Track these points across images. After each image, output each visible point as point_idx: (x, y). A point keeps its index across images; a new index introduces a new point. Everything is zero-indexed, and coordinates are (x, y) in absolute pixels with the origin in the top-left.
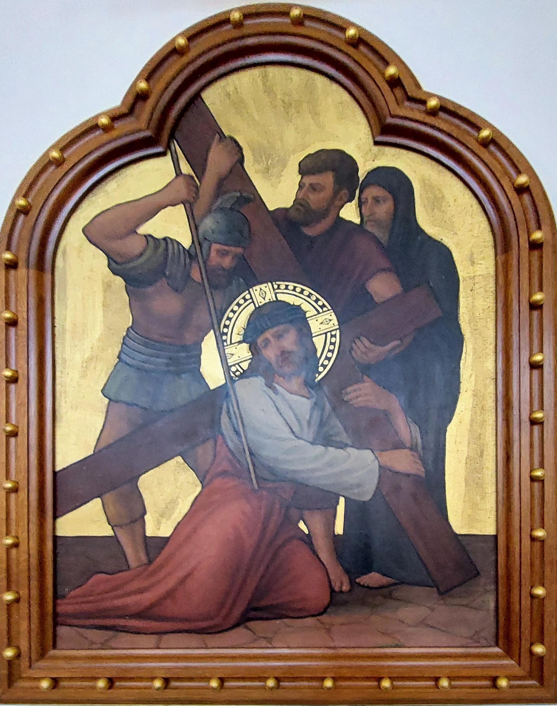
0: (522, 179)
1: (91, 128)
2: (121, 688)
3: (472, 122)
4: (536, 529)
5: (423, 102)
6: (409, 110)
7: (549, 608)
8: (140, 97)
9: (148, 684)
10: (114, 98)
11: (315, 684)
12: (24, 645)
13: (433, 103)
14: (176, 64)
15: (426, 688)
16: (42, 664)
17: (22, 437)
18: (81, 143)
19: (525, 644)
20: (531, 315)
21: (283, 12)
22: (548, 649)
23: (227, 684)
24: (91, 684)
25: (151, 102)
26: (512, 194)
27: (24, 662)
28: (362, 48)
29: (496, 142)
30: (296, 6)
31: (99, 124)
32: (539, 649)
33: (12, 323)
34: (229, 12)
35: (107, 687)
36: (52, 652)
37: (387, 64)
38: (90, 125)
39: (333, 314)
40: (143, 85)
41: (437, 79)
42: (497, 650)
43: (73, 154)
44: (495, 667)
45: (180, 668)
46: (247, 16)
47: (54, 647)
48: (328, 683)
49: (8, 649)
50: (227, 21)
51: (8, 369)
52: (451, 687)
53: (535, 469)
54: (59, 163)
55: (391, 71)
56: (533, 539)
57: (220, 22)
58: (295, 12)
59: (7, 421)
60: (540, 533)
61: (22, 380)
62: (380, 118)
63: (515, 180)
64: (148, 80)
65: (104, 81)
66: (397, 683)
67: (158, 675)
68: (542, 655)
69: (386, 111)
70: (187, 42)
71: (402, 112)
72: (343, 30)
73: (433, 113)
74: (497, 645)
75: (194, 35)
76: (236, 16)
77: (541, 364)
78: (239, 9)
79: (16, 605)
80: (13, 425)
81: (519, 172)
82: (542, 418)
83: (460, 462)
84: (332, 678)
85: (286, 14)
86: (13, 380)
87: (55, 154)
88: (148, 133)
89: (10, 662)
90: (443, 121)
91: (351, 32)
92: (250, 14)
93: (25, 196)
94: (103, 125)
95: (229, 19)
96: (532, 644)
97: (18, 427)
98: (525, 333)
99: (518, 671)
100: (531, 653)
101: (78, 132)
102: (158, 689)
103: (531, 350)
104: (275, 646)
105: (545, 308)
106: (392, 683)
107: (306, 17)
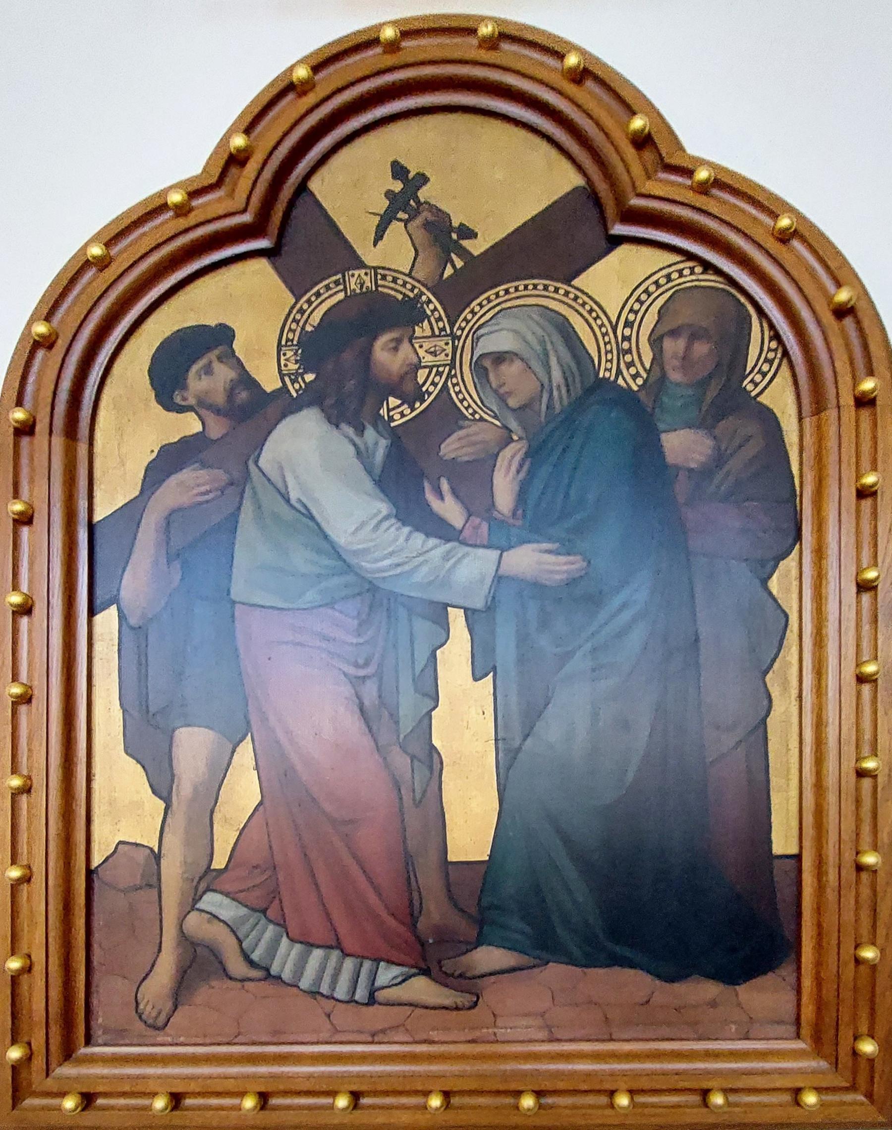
0: (843, 296)
2: (104, 1108)
3: (766, 204)
6: (665, 185)
7: (882, 980)
9: (329, 1100)
10: (192, 160)
11: (509, 1100)
12: (38, 1042)
13: (702, 174)
14: (291, 108)
15: (672, 1107)
16: (68, 1070)
17: (39, 703)
18: (146, 228)
19: (846, 1034)
22: (885, 1046)
25: (252, 167)
26: (828, 318)
27: (39, 1062)
28: (589, 84)
31: (169, 203)
32: (868, 1047)
33: (25, 520)
34: (379, 27)
35: (351, 1107)
36: (84, 1050)
42: (799, 1045)
44: (707, 1073)
45: (107, 1078)
46: (406, 34)
47: (88, 1042)
48: (528, 1102)
50: (374, 42)
52: (728, 1103)
53: (865, 758)
54: (103, 263)
55: (638, 123)
58: (485, 30)
59: (15, 678)
61: (39, 610)
64: (248, 131)
65: (172, 135)
66: (733, 1098)
68: (872, 1057)
69: (629, 189)
70: (311, 73)
71: (651, 187)
72: (561, 57)
73: (703, 189)
74: (798, 1036)
75: (322, 62)
76: (389, 33)
78: (394, 23)
80: (23, 684)
81: (839, 285)
84: (533, 1091)
85: (472, 31)
86: (26, 609)
87: (239, 141)
88: (247, 218)
89: (16, 1068)
91: (572, 60)
93: (48, 318)
94: (94, 258)
97: (31, 687)
98: (848, 540)
100: (855, 1053)
101: (135, 217)
102: (344, 1109)
104: (559, 1037)
106: (632, 1099)
107: (504, 36)
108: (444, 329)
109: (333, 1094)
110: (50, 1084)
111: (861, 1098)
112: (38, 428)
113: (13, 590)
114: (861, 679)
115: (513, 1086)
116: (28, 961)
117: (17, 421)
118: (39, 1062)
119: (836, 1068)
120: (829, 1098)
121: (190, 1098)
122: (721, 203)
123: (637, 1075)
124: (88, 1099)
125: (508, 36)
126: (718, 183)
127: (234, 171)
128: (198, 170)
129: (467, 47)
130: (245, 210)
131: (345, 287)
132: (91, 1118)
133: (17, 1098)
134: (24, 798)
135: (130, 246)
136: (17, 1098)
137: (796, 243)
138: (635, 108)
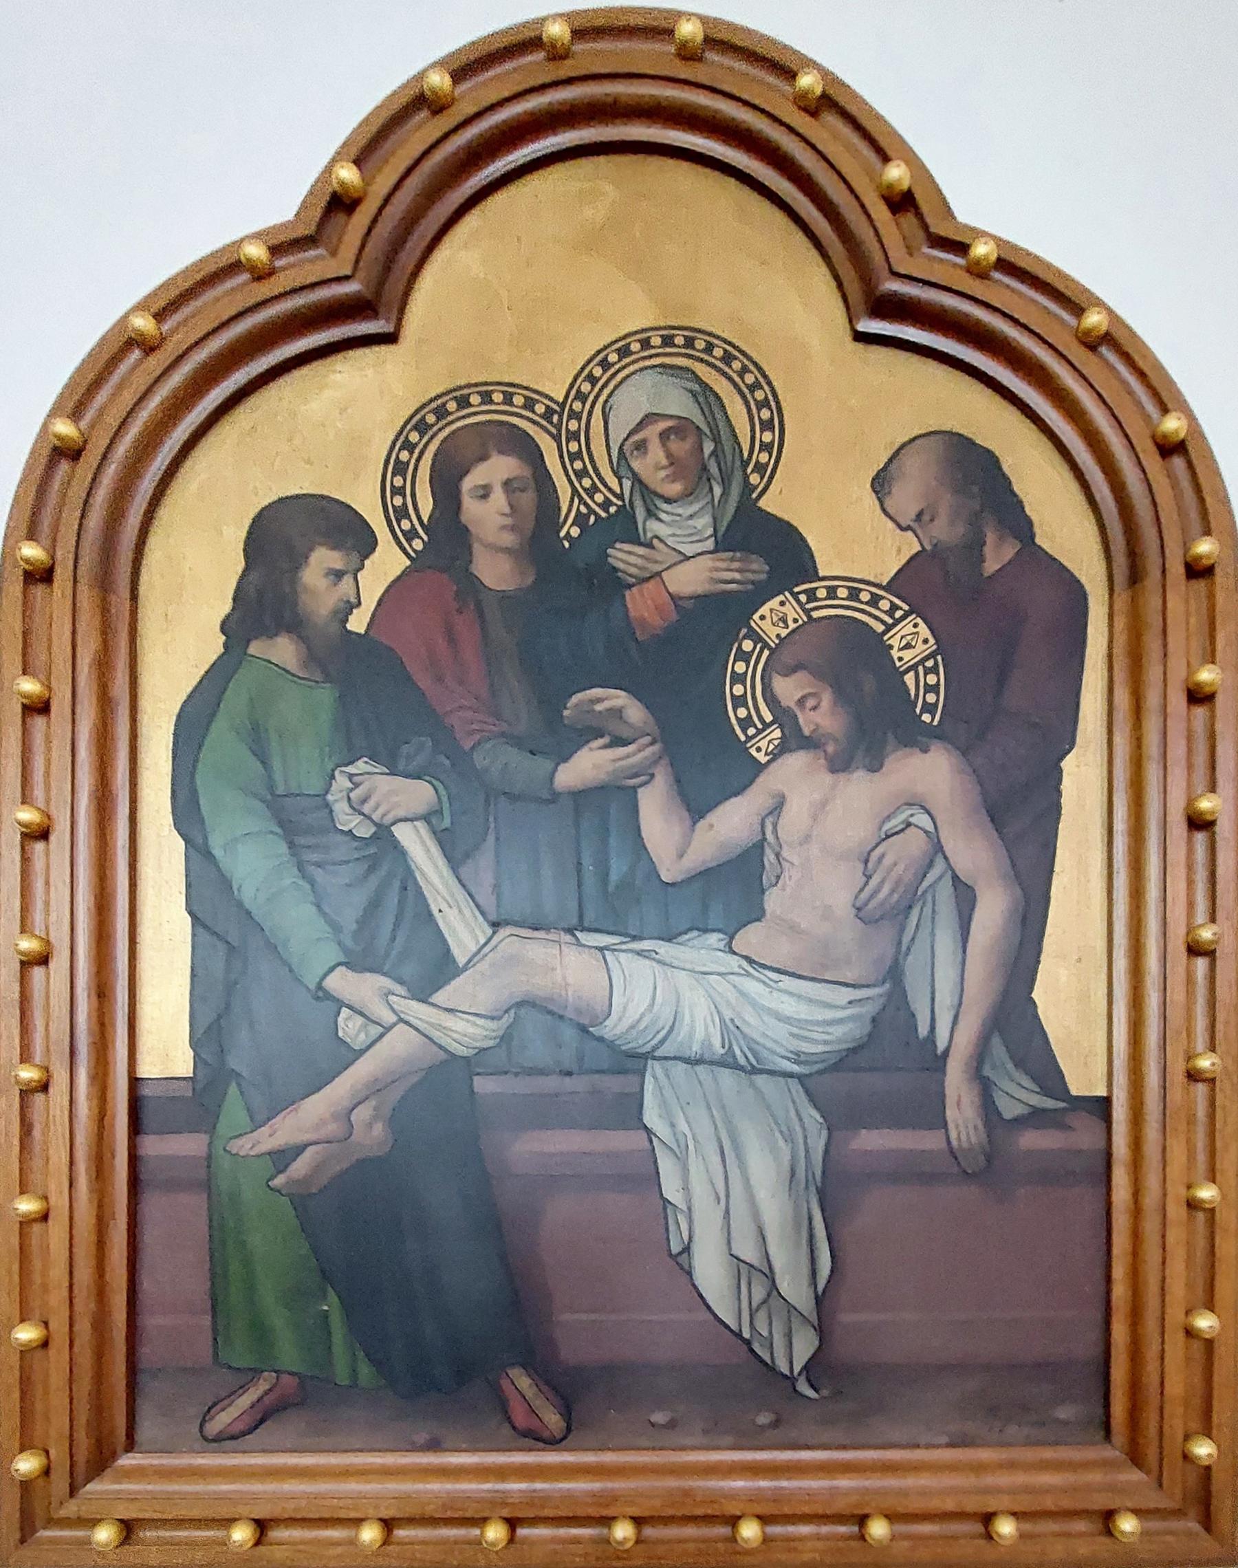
1: (224, 269)
3: (1068, 298)
4: (1199, 1185)
5: (961, 248)
8: (340, 204)
10: (281, 201)
14: (423, 131)
17: (60, 963)
19: (1175, 1314)
20: (1190, 842)
21: (657, 28)
23: (276, 1534)
24: (80, 1533)
28: (830, 119)
29: (1114, 342)
30: (690, 15)
36: (127, 1461)
37: (886, 159)
38: (224, 261)
39: (919, 620)
40: (348, 174)
41: (991, 198)
42: (1109, 1453)
43: (591, 56)
48: (623, 1531)
49: (24, 1455)
51: (25, 807)
56: (1193, 1205)
57: (522, 43)
60: (1206, 1193)
62: (867, 279)
63: (1158, 425)
66: (776, 1530)
67: (371, 1512)
72: (790, 75)
75: (467, 67)
77: (1212, 947)
79: (39, 1354)
82: (1212, 942)
83: (876, 576)
84: (381, 1520)
89: (26, 1486)
90: (1005, 292)
92: (589, 29)
95: (540, 38)
96: (1187, 1437)
99: (1154, 1500)
103: (1184, 530)
105: (1219, 699)
106: (639, 1532)
108: (894, 607)
109: (482, 1522)
110: (71, 1509)
111: (1195, 1526)
112: (58, 571)
113: (23, 803)
114: (1194, 950)
115: (224, 1512)
116: (45, 1332)
117: (27, 561)
118: (60, 1482)
119: (1161, 1485)
120: (1155, 1525)
121: (399, 1527)
122: (829, 133)
123: (777, 1497)
124: (128, 1528)
125: (723, 41)
126: (1003, 265)
127: (341, 217)
128: (289, 215)
129: (641, 55)
130: (347, 278)
131: (894, 625)
132: (131, 1554)
133: (26, 1529)
134: (39, 1098)
135: (193, 317)
136: (26, 1529)
137: (1104, 350)
138: (890, 153)
